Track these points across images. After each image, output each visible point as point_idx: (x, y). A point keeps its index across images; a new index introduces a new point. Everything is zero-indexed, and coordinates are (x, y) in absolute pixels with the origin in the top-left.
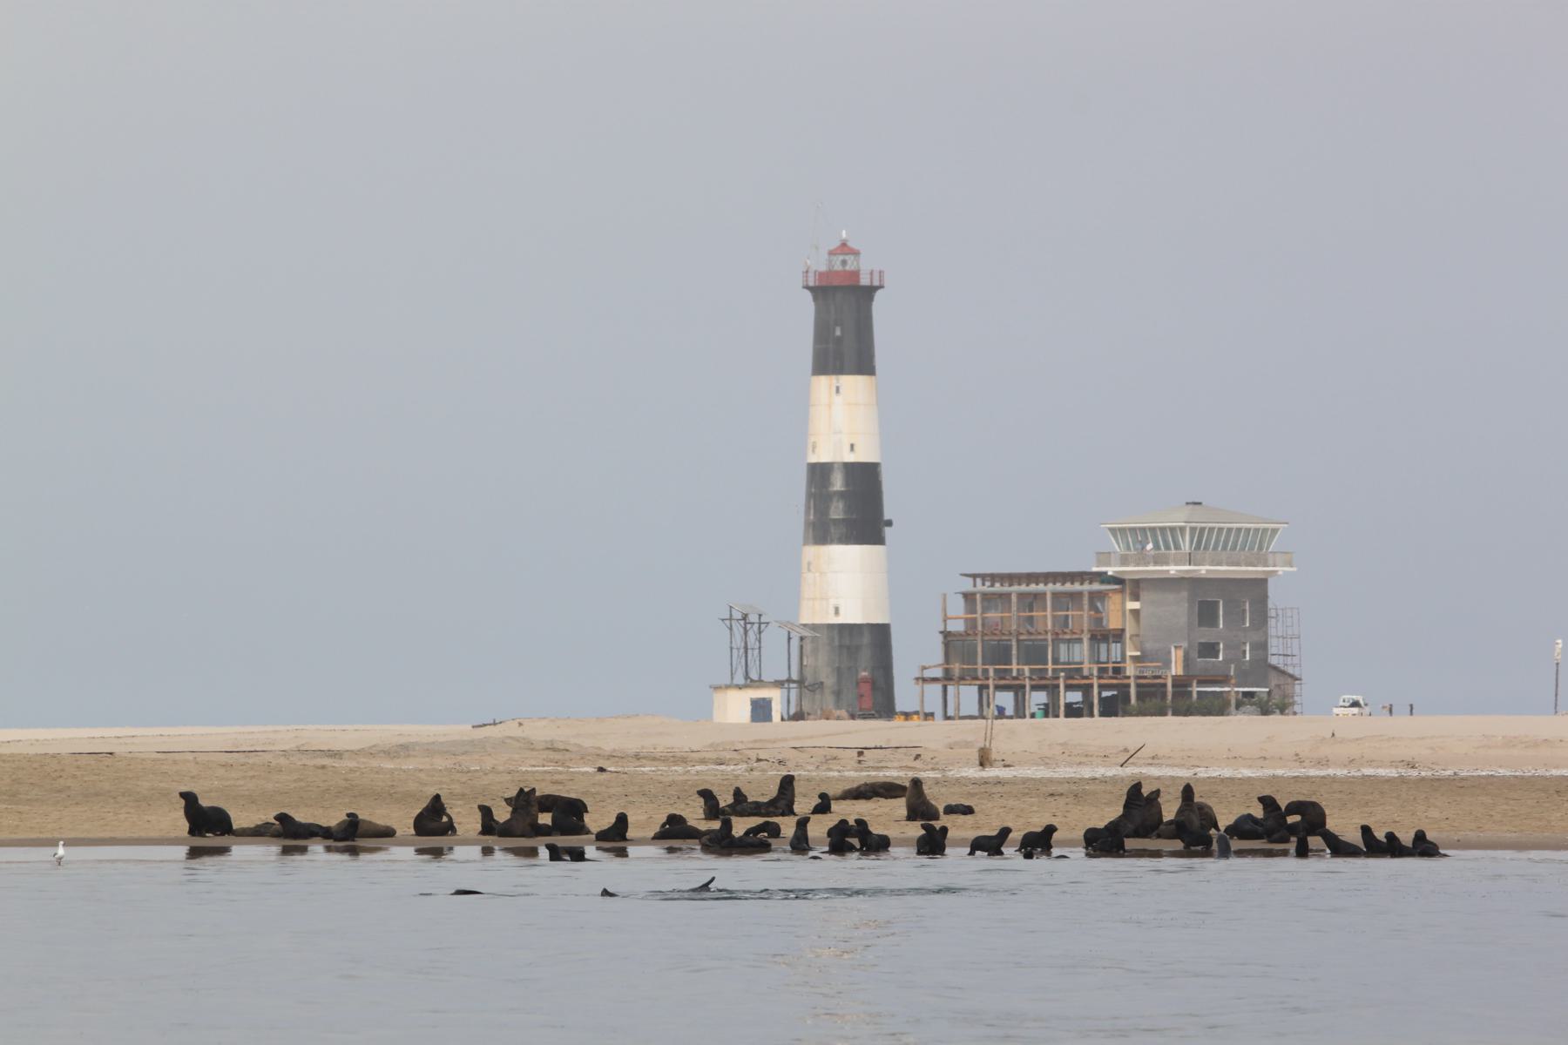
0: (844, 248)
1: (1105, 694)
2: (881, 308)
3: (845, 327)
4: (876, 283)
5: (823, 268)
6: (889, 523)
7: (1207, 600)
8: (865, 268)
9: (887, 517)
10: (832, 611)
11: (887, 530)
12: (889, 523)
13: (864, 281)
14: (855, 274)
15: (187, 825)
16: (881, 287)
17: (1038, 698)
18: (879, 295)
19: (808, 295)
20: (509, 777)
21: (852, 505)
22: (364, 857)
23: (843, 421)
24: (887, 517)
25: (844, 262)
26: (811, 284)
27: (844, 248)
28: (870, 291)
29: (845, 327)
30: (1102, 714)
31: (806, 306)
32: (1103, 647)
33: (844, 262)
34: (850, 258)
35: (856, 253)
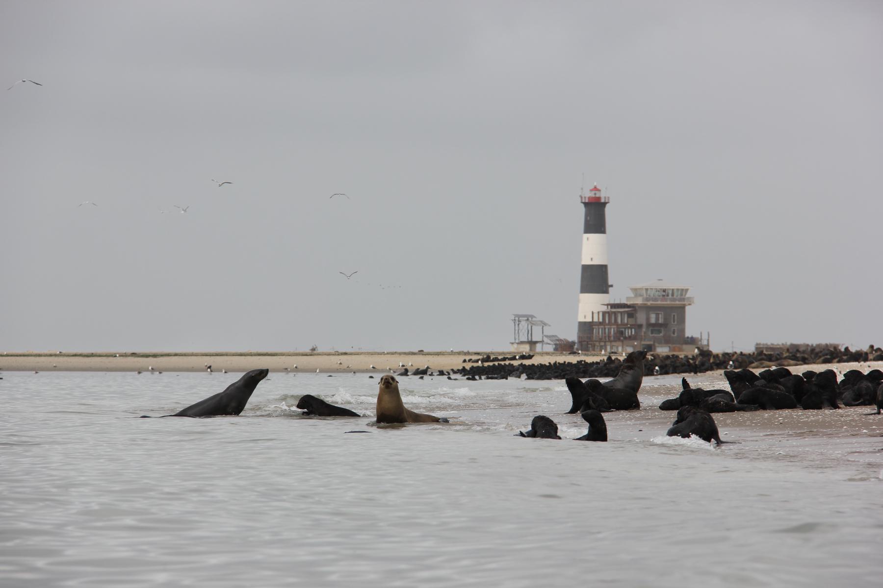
2: (608, 209)
3: (595, 216)
6: (612, 286)
7: (667, 310)
8: (603, 195)
9: (610, 283)
11: (610, 289)
12: (612, 286)
13: (603, 201)
14: (599, 198)
15: (571, 404)
17: (641, 318)
18: (607, 205)
19: (583, 205)
21: (595, 278)
23: (592, 249)
24: (610, 283)
27: (596, 189)
28: (605, 204)
29: (595, 216)
31: (582, 209)
32: (661, 321)
35: (599, 190)
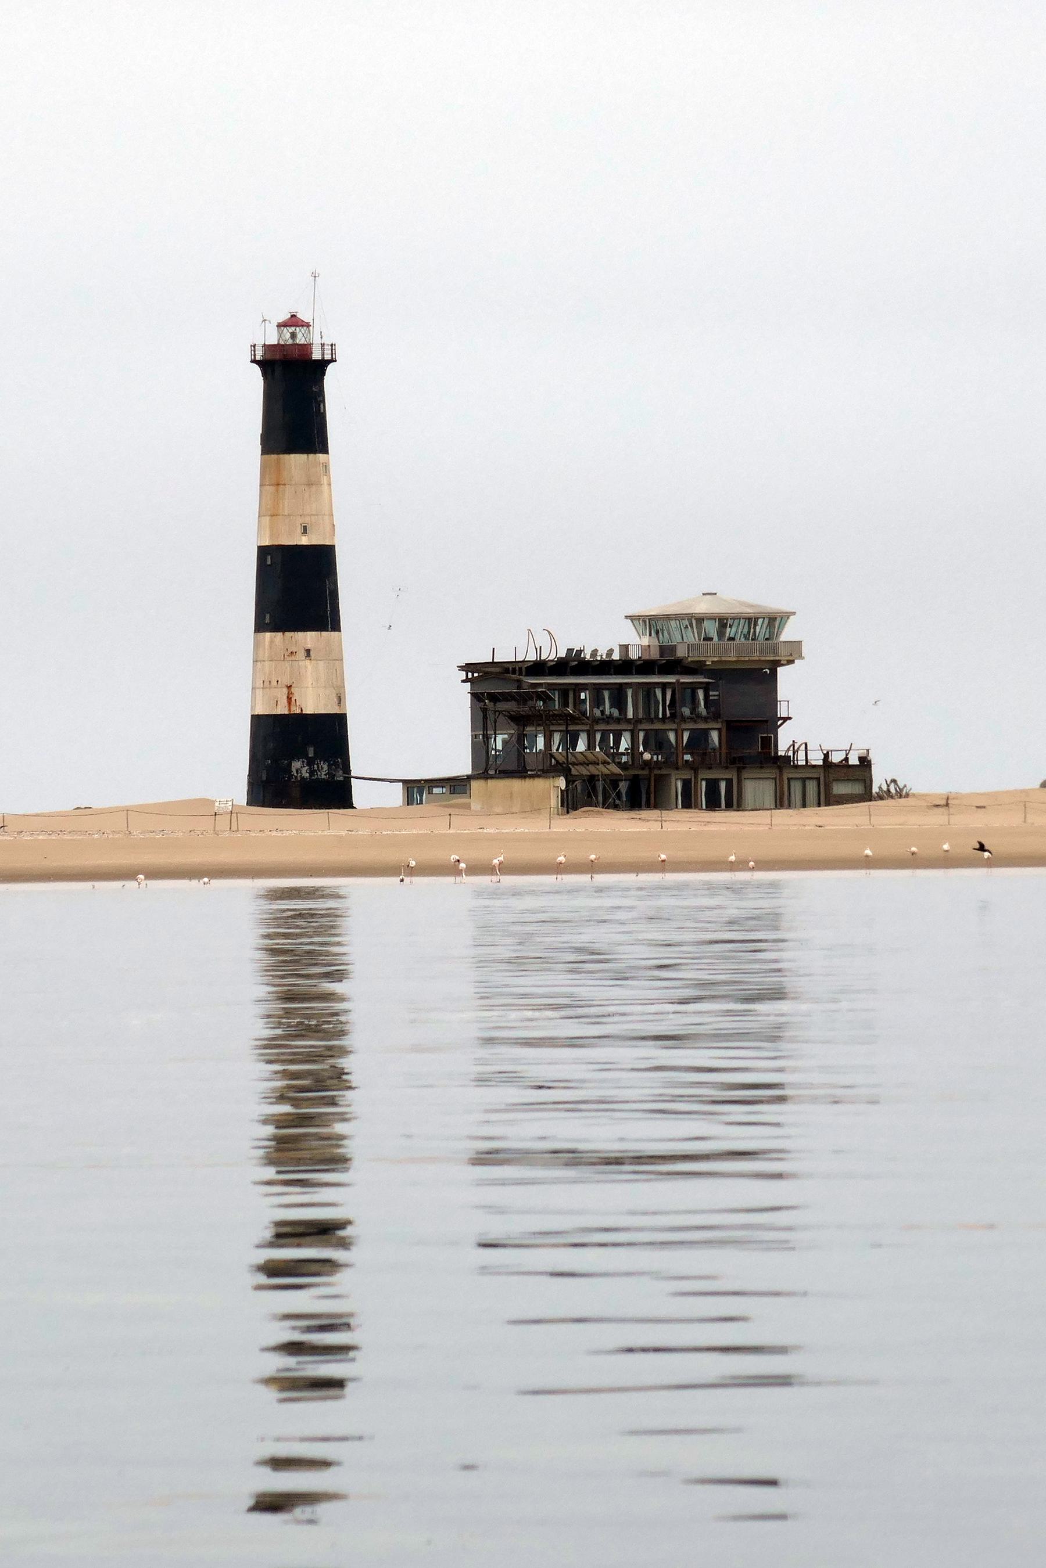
0: (293, 321)
1: (723, 785)
4: (328, 357)
5: (273, 340)
8: (318, 340)
10: (299, 530)
13: (316, 355)
14: (307, 348)
16: (333, 360)
18: (330, 369)
19: (257, 370)
20: (259, 693)
22: (69, 807)
25: (293, 335)
26: (258, 358)
27: (293, 321)
28: (322, 365)
30: (683, 807)
33: (293, 335)
34: (300, 332)
